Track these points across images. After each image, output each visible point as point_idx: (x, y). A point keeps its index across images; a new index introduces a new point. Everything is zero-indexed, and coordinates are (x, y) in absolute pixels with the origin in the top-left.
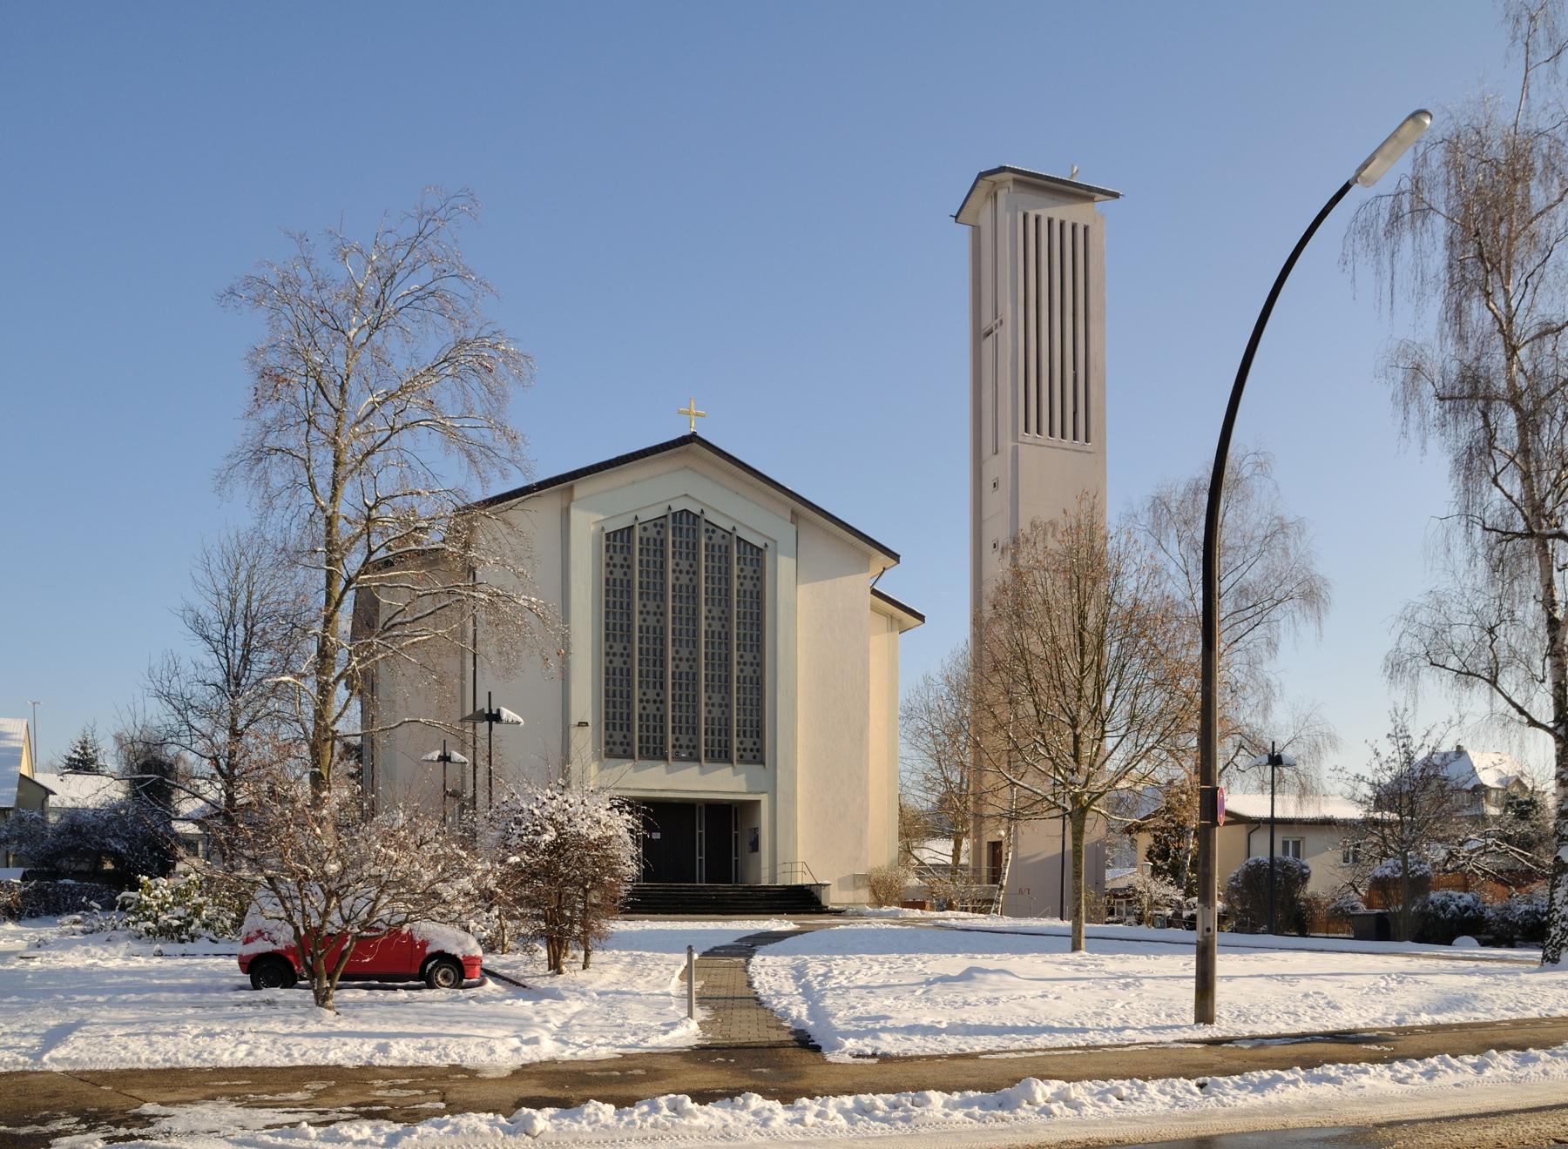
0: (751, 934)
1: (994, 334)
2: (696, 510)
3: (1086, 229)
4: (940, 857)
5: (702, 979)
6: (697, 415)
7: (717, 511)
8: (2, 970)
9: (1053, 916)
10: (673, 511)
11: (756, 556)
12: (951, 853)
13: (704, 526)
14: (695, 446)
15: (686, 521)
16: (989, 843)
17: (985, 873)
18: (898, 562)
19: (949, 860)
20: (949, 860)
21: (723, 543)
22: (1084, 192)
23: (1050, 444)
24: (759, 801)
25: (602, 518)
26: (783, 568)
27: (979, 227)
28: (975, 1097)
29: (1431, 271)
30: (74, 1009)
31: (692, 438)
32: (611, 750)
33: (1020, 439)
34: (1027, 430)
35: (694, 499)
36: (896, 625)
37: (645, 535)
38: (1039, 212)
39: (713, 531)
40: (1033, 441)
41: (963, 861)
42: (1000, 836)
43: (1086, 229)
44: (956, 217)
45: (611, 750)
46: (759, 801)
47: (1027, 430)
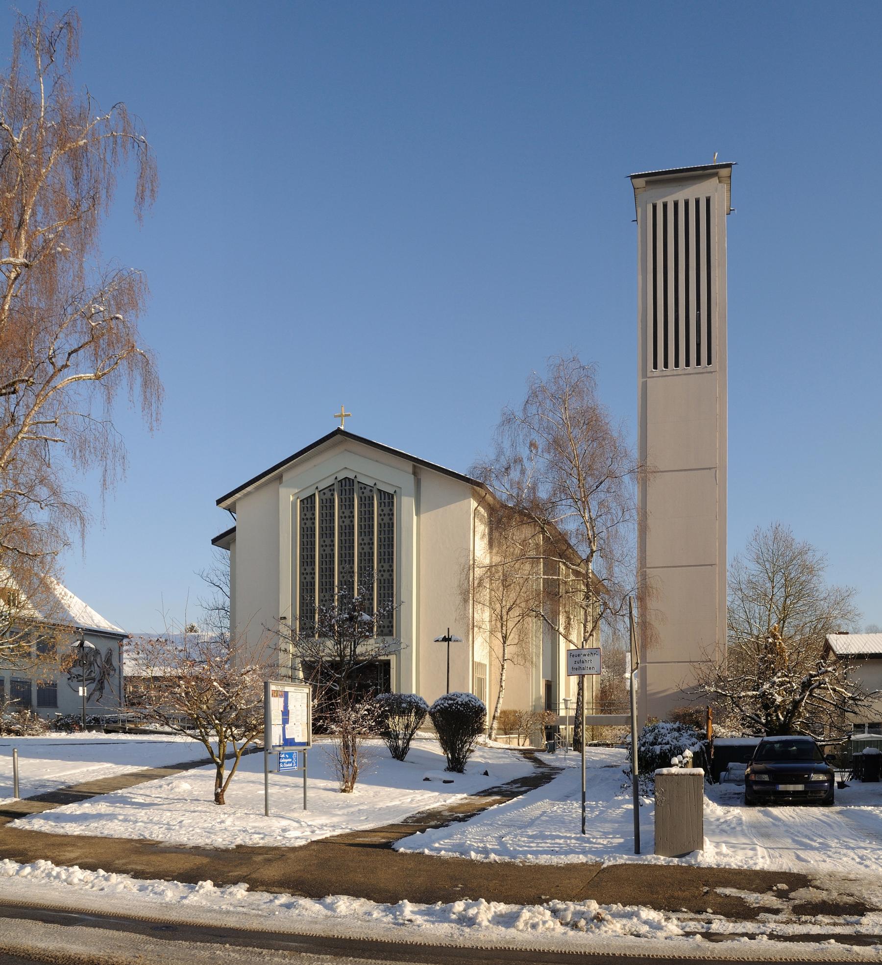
2: (352, 476)
3: (708, 200)
6: (346, 416)
7: (320, 481)
8: (868, 848)
10: (339, 479)
11: (388, 499)
13: (356, 487)
14: (338, 437)
15: (347, 485)
21: (369, 494)
22: (700, 172)
23: (709, 370)
24: (389, 661)
25: (297, 491)
26: (406, 505)
28: (667, 867)
31: (338, 431)
32: (382, 631)
33: (649, 374)
34: (655, 367)
35: (351, 470)
37: (324, 497)
38: (665, 200)
39: (365, 488)
40: (704, 370)
43: (708, 200)
45: (382, 631)
46: (389, 661)
47: (655, 367)
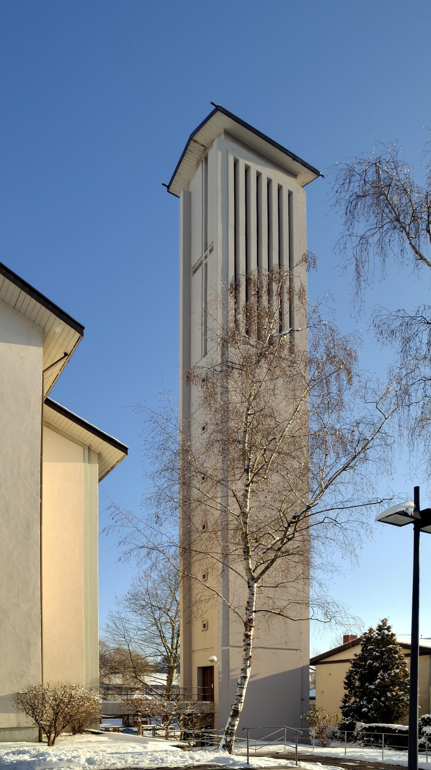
0: (404, 751)
1: (204, 265)
3: (290, 194)
4: (158, 680)
5: (49, 761)
9: (243, 691)
12: (166, 679)
16: (199, 668)
17: (195, 691)
18: (126, 453)
19: (165, 683)
20: (165, 683)
27: (190, 193)
29: (352, 629)
30: (3, 750)
36: (95, 458)
41: (174, 683)
42: (212, 661)
43: (290, 194)
44: (168, 187)
